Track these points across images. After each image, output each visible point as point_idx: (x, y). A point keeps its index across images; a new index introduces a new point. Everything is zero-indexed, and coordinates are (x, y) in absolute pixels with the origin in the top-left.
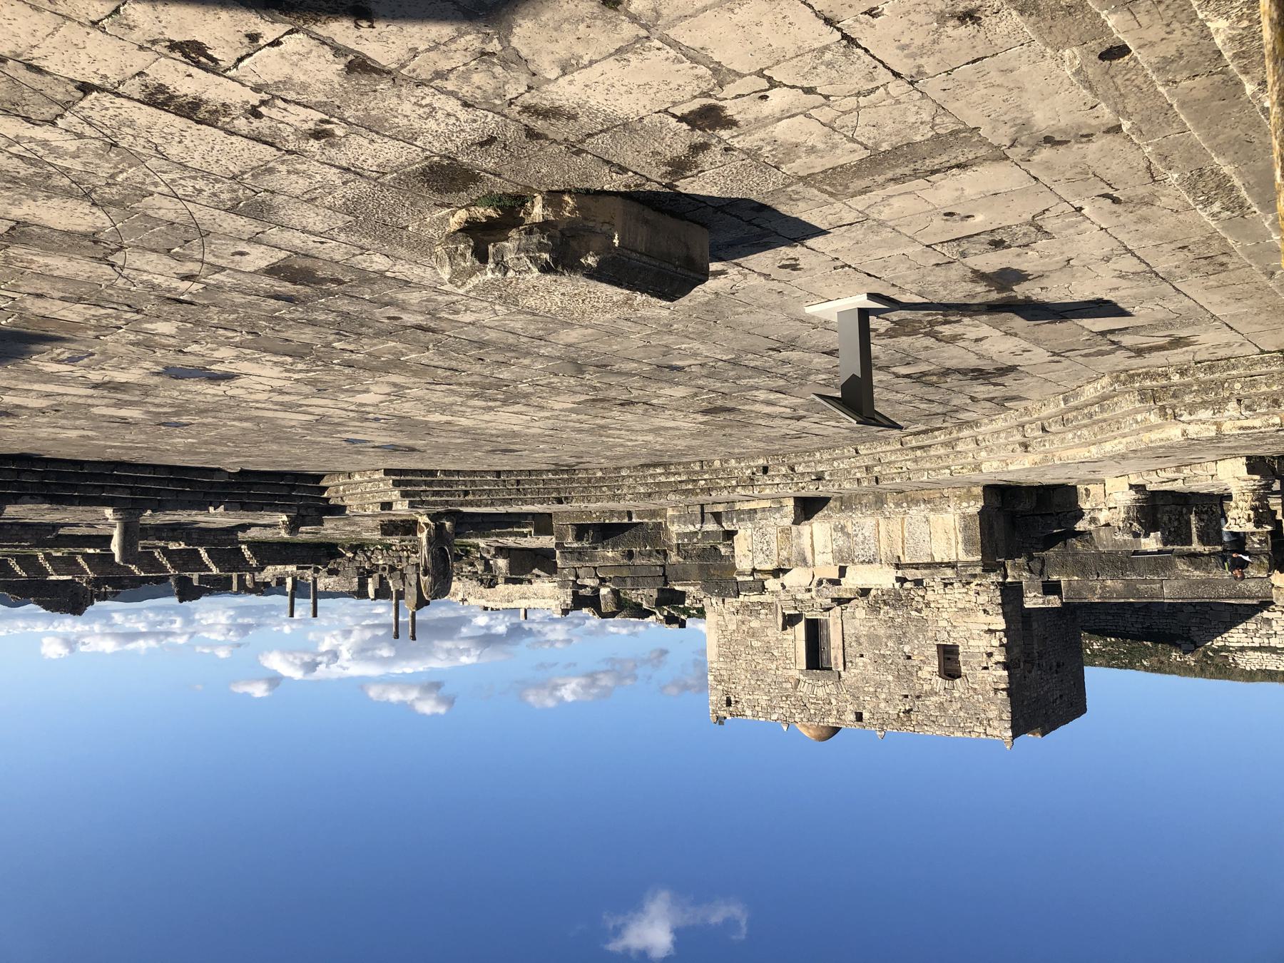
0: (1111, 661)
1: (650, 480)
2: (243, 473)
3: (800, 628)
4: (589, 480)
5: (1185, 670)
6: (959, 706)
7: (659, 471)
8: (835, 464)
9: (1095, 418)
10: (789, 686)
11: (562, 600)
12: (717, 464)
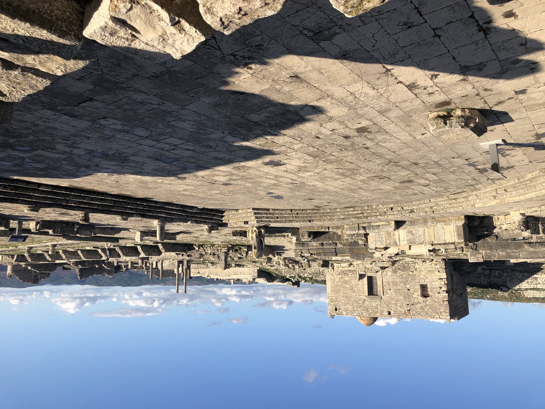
0: (475, 296)
1: (347, 213)
3: (365, 280)
4: (323, 213)
6: (429, 307)
7: (351, 209)
8: (420, 206)
9: (528, 185)
10: (361, 302)
12: (374, 207)
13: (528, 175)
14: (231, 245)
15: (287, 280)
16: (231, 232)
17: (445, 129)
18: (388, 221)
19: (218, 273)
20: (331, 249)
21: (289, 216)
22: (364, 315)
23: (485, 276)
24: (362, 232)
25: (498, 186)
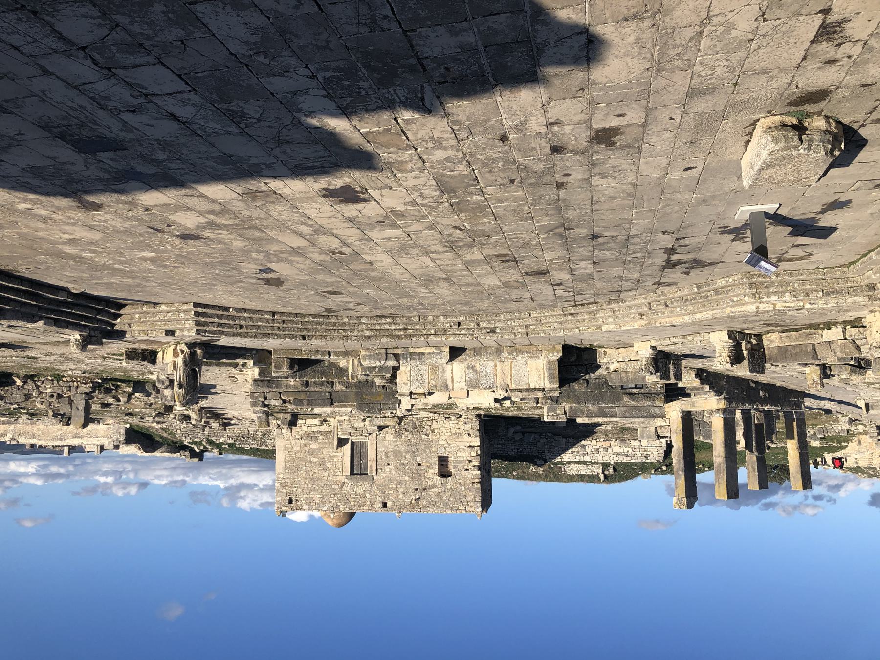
1: (378, 327)
2: (83, 296)
3: (347, 448)
4: (334, 324)
5: (537, 477)
7: (388, 320)
8: (509, 322)
9: (710, 298)
10: (337, 487)
11: (115, 438)
12: (430, 318)
13: (718, 281)
14: (101, 379)
15: (183, 448)
16: (123, 350)
17: (797, 152)
18: (438, 347)
19: (36, 435)
20: (323, 394)
21: (267, 324)
22: (341, 509)
23: (516, 441)
24: (392, 363)
25: (659, 296)
